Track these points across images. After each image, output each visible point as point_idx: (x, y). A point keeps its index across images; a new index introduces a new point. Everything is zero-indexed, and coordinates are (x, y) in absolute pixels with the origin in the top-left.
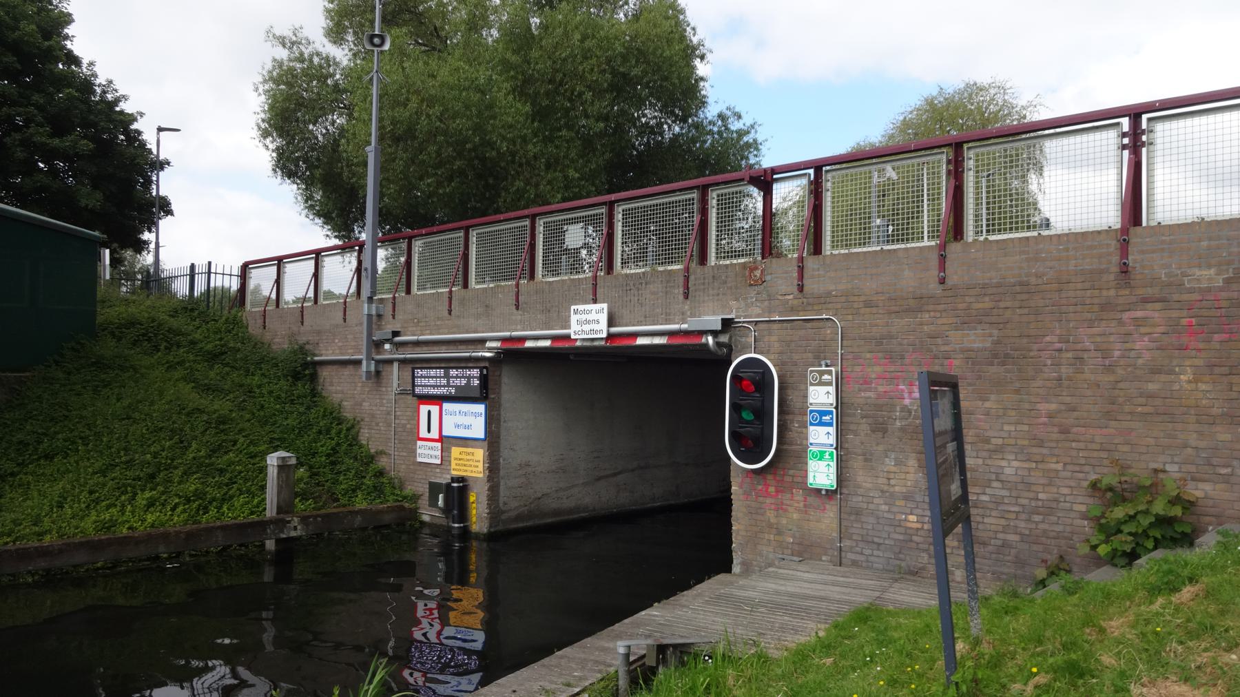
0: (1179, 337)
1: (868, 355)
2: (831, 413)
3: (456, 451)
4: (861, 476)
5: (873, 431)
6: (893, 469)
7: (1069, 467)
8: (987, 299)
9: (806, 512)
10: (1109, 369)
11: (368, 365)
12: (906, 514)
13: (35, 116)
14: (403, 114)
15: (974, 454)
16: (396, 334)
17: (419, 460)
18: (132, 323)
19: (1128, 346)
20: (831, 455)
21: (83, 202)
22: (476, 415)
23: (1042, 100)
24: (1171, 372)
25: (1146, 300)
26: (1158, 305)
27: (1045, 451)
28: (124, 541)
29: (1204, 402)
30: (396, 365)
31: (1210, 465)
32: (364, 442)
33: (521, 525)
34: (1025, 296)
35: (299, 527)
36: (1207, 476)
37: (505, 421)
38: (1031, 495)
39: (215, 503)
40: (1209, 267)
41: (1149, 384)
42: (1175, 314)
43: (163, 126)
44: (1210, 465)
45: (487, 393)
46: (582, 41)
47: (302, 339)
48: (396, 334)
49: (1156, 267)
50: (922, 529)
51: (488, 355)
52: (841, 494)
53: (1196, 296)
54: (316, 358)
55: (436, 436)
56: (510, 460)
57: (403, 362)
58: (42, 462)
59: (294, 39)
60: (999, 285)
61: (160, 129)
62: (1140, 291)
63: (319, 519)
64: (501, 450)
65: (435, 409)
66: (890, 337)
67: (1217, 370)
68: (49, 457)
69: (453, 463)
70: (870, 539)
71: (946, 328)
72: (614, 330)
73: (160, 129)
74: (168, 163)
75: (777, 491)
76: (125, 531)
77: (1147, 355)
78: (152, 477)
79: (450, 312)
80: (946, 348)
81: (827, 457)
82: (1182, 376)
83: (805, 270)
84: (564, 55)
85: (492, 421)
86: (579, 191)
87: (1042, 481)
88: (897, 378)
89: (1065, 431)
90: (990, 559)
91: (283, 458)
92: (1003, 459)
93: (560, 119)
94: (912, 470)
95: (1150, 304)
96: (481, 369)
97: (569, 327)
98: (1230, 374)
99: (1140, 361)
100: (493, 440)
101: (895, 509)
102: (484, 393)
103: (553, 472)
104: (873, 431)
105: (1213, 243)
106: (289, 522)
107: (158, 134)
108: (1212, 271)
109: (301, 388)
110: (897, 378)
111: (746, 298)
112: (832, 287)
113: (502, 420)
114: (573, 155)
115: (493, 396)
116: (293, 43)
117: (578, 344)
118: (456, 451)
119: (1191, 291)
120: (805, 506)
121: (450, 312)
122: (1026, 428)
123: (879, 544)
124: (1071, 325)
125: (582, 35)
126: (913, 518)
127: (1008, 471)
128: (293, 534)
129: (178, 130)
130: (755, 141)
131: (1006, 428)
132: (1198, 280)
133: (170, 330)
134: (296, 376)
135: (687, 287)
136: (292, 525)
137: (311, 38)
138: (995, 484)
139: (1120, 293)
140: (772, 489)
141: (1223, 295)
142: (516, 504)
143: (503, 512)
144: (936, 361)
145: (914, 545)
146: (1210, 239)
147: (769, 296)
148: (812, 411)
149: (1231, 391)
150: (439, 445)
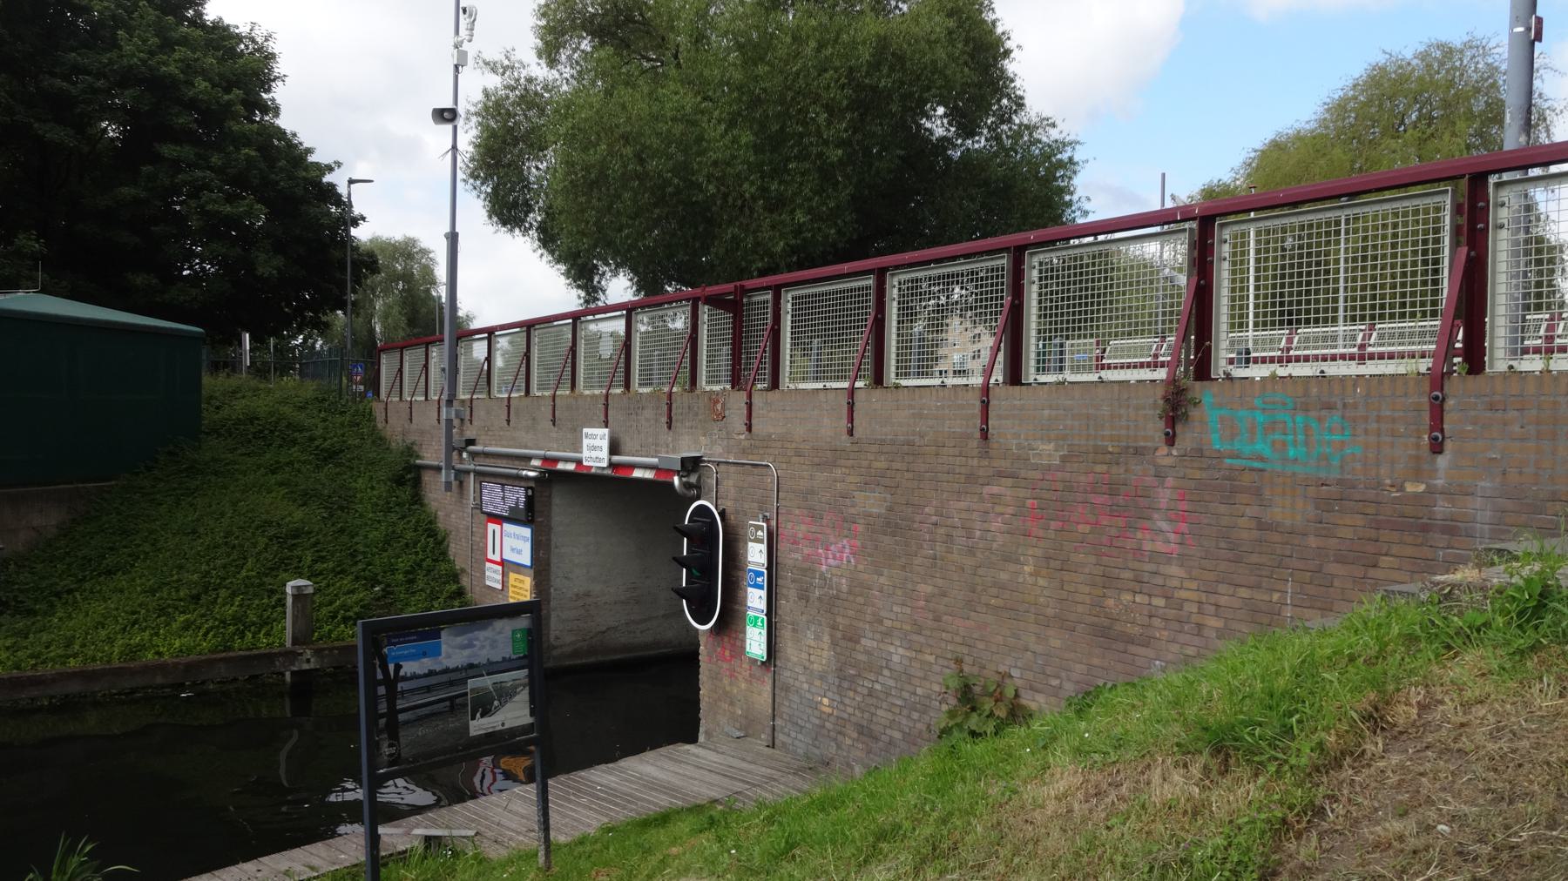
0: (1024, 521)
1: (797, 512)
2: (761, 574)
3: (512, 576)
4: (788, 648)
5: (800, 599)
6: (813, 643)
7: (941, 661)
8: (883, 458)
9: (751, 684)
10: (971, 551)
11: (447, 475)
12: (822, 697)
13: (212, 180)
14: (593, 157)
15: (871, 635)
16: (471, 442)
17: (488, 583)
18: (252, 419)
19: (986, 525)
20: (762, 622)
21: (260, 270)
22: (524, 539)
23: (1547, 61)
24: (1017, 562)
25: (1001, 474)
26: (1010, 481)
27: (922, 639)
28: (147, 669)
29: (1042, 600)
30: (472, 475)
31: (1044, 673)
32: (452, 558)
33: (578, 662)
34: (911, 458)
35: (312, 660)
36: (1040, 686)
37: (556, 547)
38: (910, 688)
39: (253, 628)
40: (1049, 441)
41: (1001, 573)
42: (1022, 493)
43: (354, 178)
44: (1044, 673)
45: (533, 516)
46: (818, 50)
47: (411, 438)
48: (471, 442)
49: (1009, 436)
50: (832, 714)
51: (532, 474)
52: (775, 666)
53: (1037, 475)
54: (418, 461)
55: (499, 560)
56: (564, 590)
57: (478, 474)
58: (102, 579)
59: (506, 63)
60: (893, 443)
61: (351, 182)
62: (996, 463)
63: (336, 652)
64: (552, 578)
65: (497, 527)
66: (812, 492)
67: (1053, 564)
68: (109, 573)
69: (511, 589)
70: (795, 719)
71: (852, 487)
72: (616, 458)
73: (351, 182)
74: (363, 219)
75: (732, 656)
76: (150, 656)
77: (1000, 539)
78: (196, 598)
79: (508, 421)
80: (852, 511)
81: (759, 624)
82: (1025, 568)
83: (753, 408)
84: (794, 69)
85: (538, 546)
86: (813, 236)
87: (920, 674)
88: (817, 540)
89: (937, 619)
90: (880, 756)
91: (299, 588)
92: (892, 644)
93: (792, 147)
94: (826, 647)
95: (1004, 479)
96: (527, 489)
97: (581, 452)
98: (1062, 570)
99: (995, 545)
100: (541, 567)
101: (813, 690)
102: (529, 515)
103: (622, 602)
104: (800, 599)
105: (1054, 413)
106: (301, 654)
107: (349, 187)
108: (1051, 446)
109: (405, 493)
110: (817, 540)
111: (711, 434)
112: (772, 431)
113: (553, 547)
114: (807, 191)
115: (540, 519)
116: (505, 68)
117: (593, 471)
118: (512, 576)
119: (1036, 468)
120: (750, 675)
121: (508, 421)
122: (908, 610)
123: (802, 727)
124: (944, 496)
125: (818, 42)
126: (826, 701)
127: (896, 659)
128: (306, 667)
129: (371, 181)
130: (1071, 159)
131: (895, 609)
132: (1040, 455)
133: (289, 426)
134: (399, 481)
135: (670, 417)
136: (304, 658)
137: (526, 61)
138: (886, 672)
139: (982, 464)
140: (727, 653)
141: (1059, 475)
142: (574, 638)
143: (555, 648)
144: (845, 524)
145: (826, 732)
146: (1051, 408)
147: (727, 433)
148: (750, 571)
149: (1062, 589)
150: (500, 568)
